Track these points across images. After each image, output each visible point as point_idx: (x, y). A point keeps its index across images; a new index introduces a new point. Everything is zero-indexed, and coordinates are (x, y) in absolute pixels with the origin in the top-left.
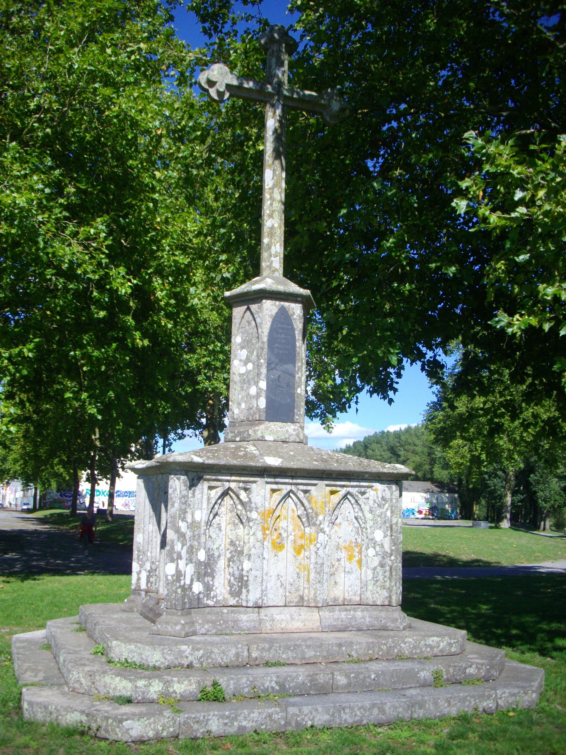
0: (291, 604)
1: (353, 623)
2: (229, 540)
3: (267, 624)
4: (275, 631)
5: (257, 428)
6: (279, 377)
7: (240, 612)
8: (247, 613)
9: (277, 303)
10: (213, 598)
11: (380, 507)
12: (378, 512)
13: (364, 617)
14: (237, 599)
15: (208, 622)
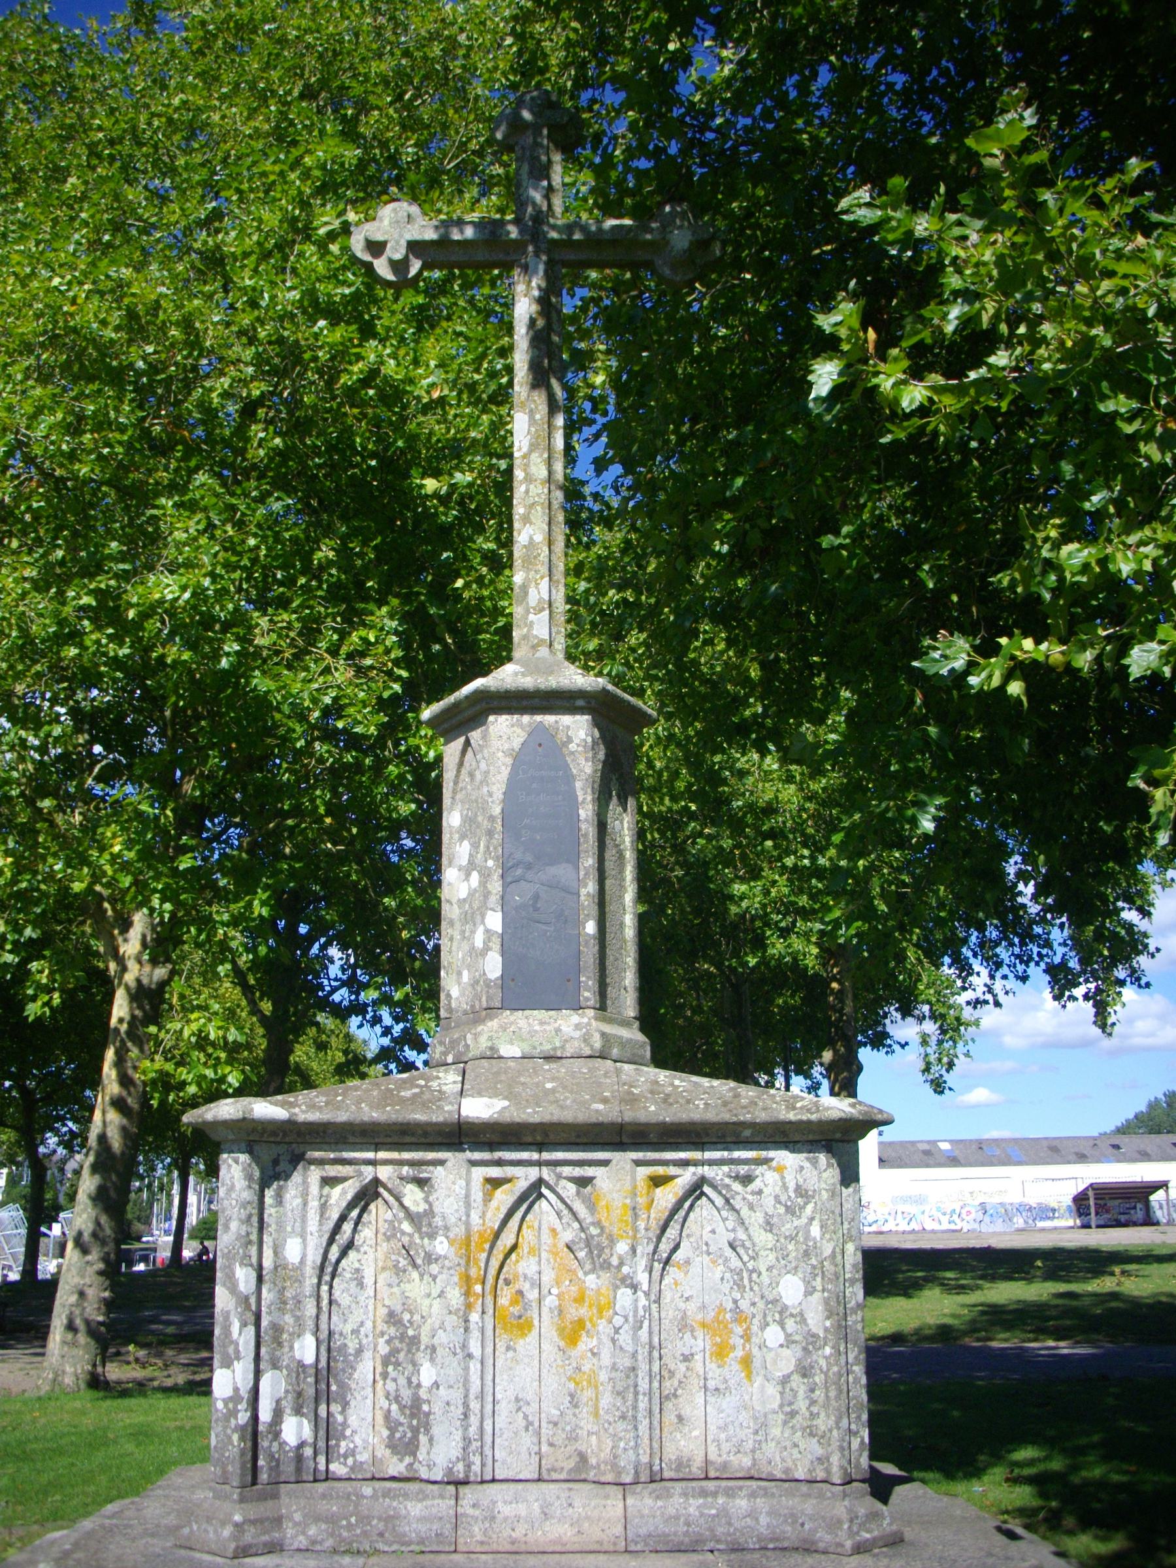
0: (555, 1476)
1: (720, 1530)
2: (385, 1311)
3: (476, 1529)
4: (495, 1547)
5: (480, 1028)
6: (536, 897)
7: (406, 1496)
8: (426, 1497)
9: (526, 719)
10: (345, 1456)
11: (793, 1214)
12: (787, 1228)
13: (752, 1514)
14: (408, 1460)
15: (317, 1519)
